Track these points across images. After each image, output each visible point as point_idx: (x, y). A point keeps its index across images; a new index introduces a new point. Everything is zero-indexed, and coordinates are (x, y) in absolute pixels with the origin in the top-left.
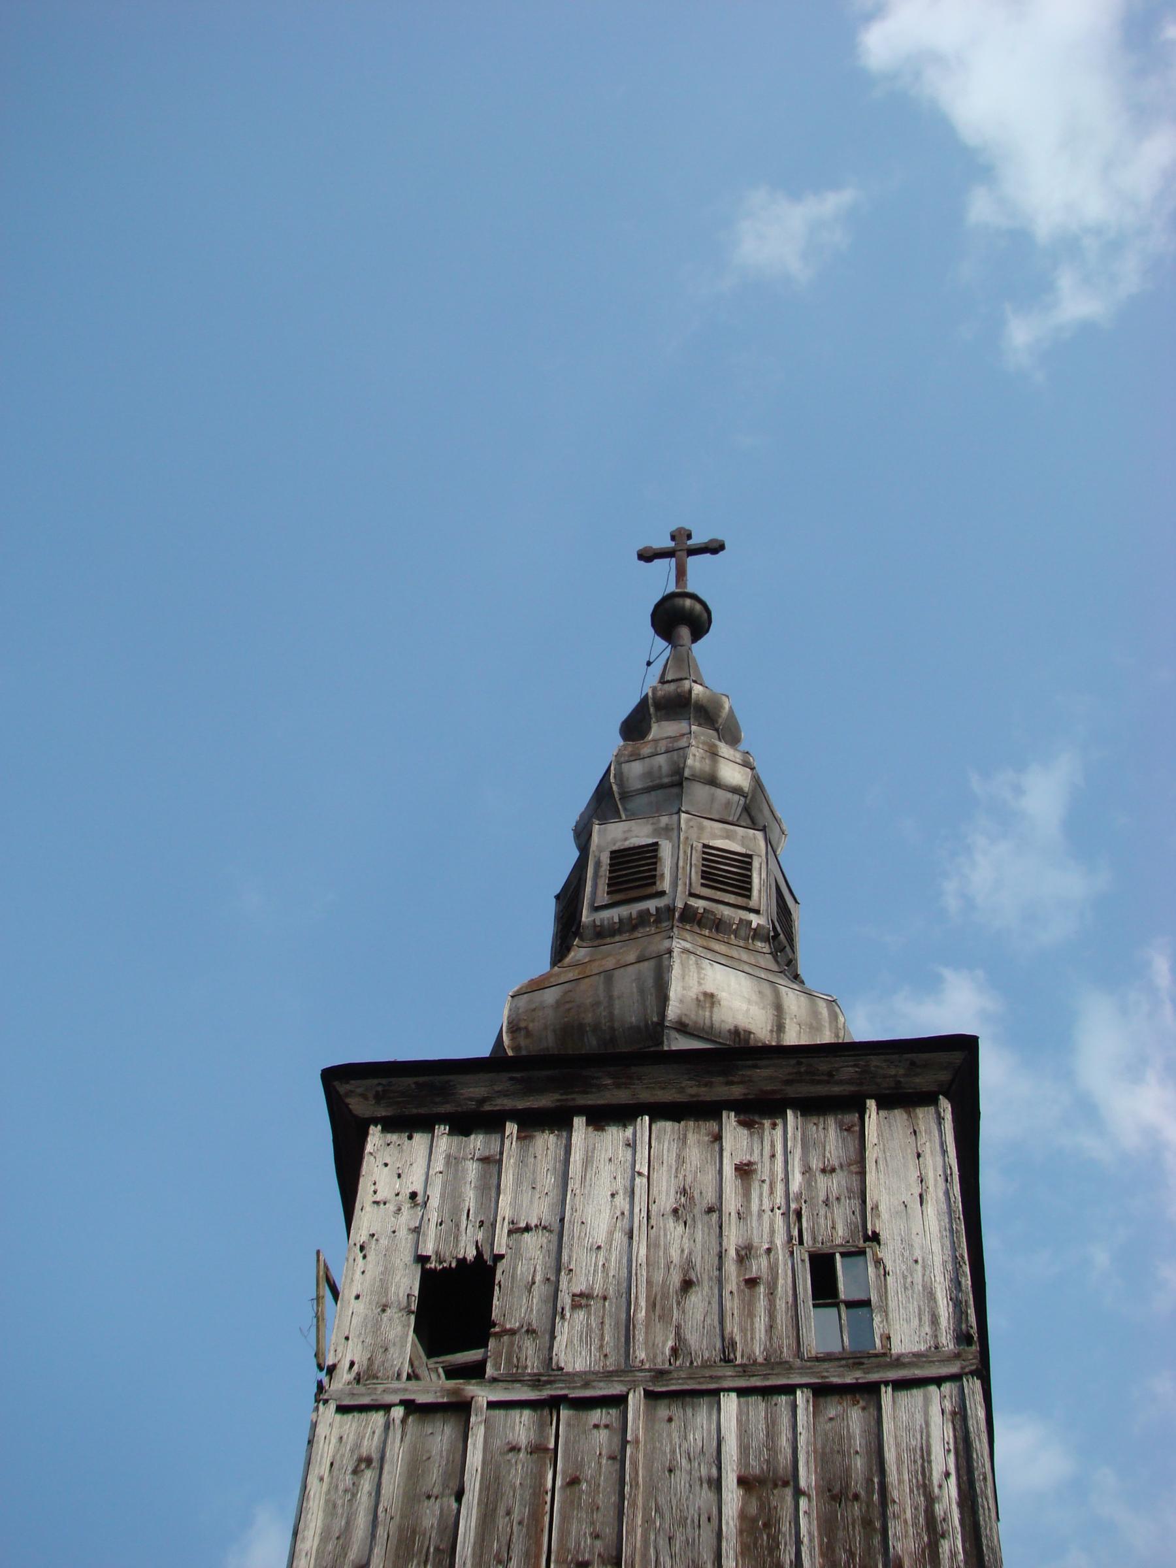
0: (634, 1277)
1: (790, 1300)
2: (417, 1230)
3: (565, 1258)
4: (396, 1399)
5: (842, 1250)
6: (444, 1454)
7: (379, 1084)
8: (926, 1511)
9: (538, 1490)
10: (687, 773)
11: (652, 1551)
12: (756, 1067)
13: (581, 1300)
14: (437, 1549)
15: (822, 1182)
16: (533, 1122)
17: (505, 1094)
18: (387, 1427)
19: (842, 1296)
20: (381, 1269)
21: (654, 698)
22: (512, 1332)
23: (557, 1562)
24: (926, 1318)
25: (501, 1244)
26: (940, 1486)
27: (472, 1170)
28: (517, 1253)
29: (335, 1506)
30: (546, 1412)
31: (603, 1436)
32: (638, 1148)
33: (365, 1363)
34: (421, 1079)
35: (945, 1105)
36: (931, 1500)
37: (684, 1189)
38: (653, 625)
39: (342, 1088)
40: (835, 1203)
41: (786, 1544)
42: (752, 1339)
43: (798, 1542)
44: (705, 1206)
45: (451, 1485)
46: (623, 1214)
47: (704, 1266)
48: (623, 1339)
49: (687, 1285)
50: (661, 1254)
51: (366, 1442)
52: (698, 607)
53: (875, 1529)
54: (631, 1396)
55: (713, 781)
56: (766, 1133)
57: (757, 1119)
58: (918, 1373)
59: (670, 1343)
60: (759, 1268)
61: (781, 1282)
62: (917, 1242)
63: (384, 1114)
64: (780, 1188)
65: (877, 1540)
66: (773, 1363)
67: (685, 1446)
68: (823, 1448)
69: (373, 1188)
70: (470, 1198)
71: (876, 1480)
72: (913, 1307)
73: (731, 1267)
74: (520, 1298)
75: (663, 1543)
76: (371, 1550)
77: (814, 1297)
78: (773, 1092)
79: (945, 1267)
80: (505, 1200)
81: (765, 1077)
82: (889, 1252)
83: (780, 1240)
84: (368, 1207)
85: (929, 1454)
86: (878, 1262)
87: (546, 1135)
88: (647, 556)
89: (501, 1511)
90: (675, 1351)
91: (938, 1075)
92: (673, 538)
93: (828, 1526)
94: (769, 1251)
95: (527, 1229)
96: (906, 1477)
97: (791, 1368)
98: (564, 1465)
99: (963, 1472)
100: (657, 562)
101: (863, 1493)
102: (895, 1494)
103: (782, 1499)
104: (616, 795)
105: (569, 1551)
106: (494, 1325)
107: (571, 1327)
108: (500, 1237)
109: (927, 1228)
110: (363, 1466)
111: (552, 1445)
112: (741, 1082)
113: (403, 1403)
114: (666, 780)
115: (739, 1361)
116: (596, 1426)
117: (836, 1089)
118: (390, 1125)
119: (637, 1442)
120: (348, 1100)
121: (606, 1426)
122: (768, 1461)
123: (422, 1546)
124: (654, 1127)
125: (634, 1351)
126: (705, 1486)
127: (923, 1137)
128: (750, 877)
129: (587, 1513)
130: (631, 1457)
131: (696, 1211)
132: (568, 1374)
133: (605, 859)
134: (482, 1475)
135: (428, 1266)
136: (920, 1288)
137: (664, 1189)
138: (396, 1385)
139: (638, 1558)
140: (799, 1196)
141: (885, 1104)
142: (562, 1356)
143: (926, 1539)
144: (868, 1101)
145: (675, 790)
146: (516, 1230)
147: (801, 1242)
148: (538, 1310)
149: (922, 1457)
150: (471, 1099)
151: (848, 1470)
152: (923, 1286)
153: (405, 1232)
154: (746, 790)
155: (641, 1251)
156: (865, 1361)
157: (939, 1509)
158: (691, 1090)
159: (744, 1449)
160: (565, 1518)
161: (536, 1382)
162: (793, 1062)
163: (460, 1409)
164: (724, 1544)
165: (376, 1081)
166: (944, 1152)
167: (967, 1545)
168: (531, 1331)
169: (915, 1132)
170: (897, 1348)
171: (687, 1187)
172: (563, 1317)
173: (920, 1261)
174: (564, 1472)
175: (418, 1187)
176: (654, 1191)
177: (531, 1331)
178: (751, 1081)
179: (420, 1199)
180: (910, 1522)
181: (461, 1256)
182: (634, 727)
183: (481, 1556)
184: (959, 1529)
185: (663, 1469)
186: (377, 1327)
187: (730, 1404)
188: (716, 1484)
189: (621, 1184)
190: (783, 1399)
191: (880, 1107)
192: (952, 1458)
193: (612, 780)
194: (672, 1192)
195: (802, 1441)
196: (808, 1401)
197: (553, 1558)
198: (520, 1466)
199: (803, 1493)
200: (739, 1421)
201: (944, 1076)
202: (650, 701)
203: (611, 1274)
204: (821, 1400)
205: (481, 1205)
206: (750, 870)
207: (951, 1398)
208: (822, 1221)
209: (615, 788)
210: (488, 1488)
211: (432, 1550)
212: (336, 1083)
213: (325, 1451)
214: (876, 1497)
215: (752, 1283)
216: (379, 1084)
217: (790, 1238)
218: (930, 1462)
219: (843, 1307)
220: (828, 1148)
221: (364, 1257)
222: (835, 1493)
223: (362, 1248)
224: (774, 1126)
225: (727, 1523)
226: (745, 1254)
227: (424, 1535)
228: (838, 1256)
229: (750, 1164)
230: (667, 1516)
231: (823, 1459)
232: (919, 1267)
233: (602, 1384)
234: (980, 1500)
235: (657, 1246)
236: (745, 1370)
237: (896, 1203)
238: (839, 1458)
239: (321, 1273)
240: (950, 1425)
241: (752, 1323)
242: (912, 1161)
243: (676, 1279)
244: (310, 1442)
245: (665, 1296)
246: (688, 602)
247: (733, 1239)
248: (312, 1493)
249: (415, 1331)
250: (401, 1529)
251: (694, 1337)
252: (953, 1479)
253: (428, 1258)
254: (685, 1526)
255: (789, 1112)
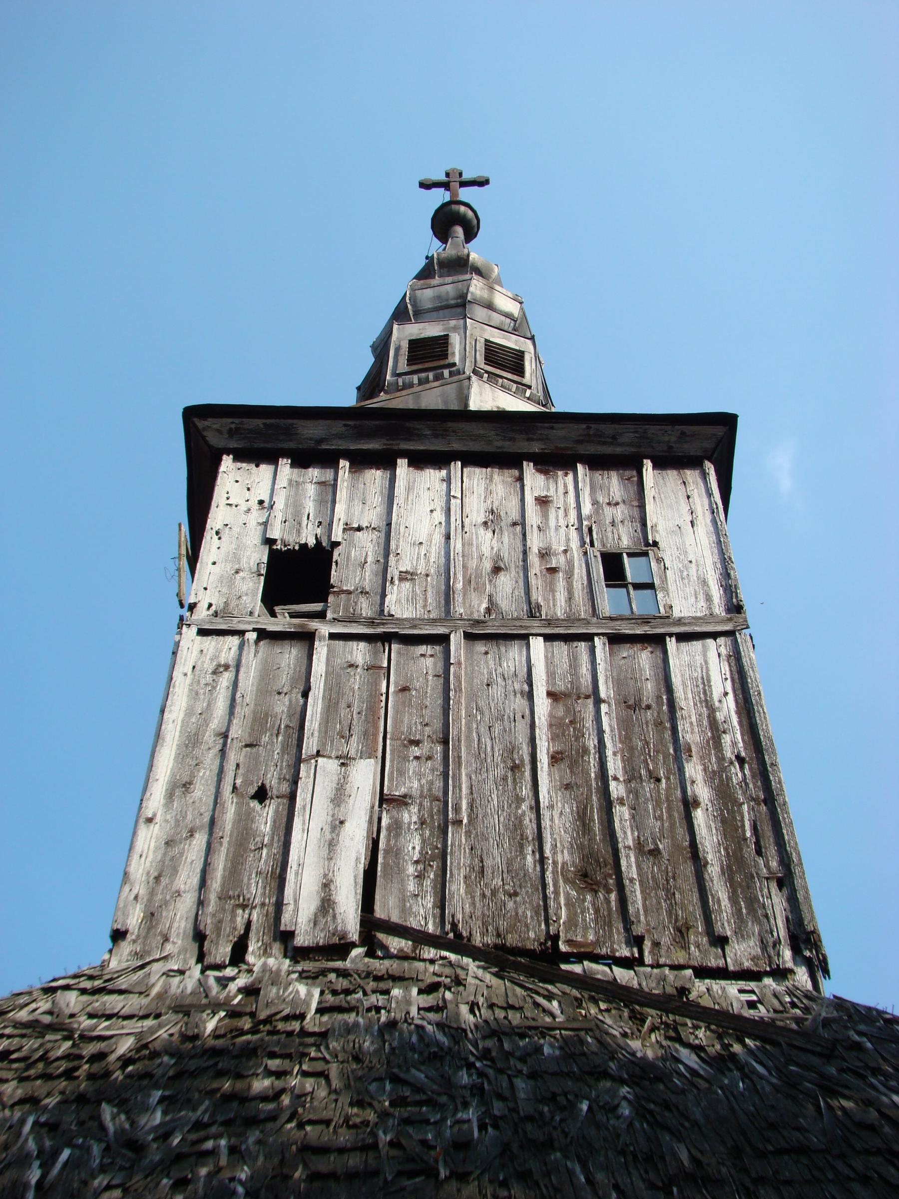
0: (452, 561)
1: (585, 583)
2: (265, 524)
3: (393, 545)
4: (250, 627)
5: (628, 551)
6: (292, 666)
7: (232, 423)
8: (709, 717)
9: (374, 694)
10: (469, 298)
11: (474, 734)
12: (552, 428)
13: (405, 576)
14: (287, 726)
15: (608, 512)
16: (362, 461)
17: (340, 436)
18: (241, 647)
19: (630, 580)
20: (234, 546)
21: (438, 259)
22: (349, 592)
23: (392, 739)
24: (701, 597)
25: (337, 534)
26: (720, 701)
27: (311, 490)
28: (351, 543)
29: (197, 694)
30: (379, 644)
31: (429, 662)
32: (453, 481)
33: (222, 605)
34: (269, 421)
35: (710, 468)
36: (712, 710)
37: (492, 510)
38: (432, 228)
39: (200, 424)
40: (620, 524)
41: (589, 735)
42: (554, 605)
43: (600, 732)
44: (510, 521)
45: (298, 686)
46: (440, 523)
47: (511, 556)
48: (443, 602)
49: (497, 570)
50: (474, 549)
51: (223, 655)
52: (470, 214)
53: (665, 728)
54: (452, 636)
55: (490, 306)
56: (560, 478)
57: (551, 468)
58: (698, 629)
59: (484, 605)
60: (558, 562)
61: (576, 571)
62: (690, 550)
63: (236, 446)
64: (573, 514)
65: (668, 735)
66: (571, 619)
67: (499, 670)
68: (619, 675)
69: (226, 495)
70: (310, 506)
71: (664, 697)
72: (689, 590)
73: (534, 559)
74: (355, 571)
75: (483, 730)
76: (230, 721)
77: (607, 579)
78: (566, 448)
79: (715, 566)
80: (340, 508)
81: (560, 435)
82: (668, 550)
83: (575, 544)
84: (222, 507)
85: (709, 681)
86: (659, 560)
87: (373, 471)
88: (426, 185)
89: (343, 705)
90: (488, 611)
91: (702, 443)
92: (447, 175)
93: (626, 727)
94: (565, 551)
95: (359, 529)
96: (690, 696)
97: (589, 623)
98: (396, 678)
99: (739, 692)
100: (434, 190)
101: (654, 705)
102: (683, 704)
103: (585, 706)
104: (411, 312)
105: (402, 733)
106: (333, 587)
107: (399, 592)
108: (337, 531)
109: (698, 541)
110: (221, 669)
111: (385, 665)
112: (539, 439)
113: (254, 630)
114: (452, 302)
115: (544, 617)
116: (422, 655)
117: (618, 450)
118: (241, 456)
119: (459, 663)
120: (205, 433)
121: (432, 656)
122: (572, 682)
123: (274, 724)
124: (465, 470)
125: (454, 608)
126: (518, 695)
127: (691, 487)
128: (523, 365)
129: (417, 710)
130: (454, 674)
131: (503, 524)
132: (397, 619)
133: (405, 345)
134: (326, 680)
135: (275, 547)
136: (696, 579)
137: (475, 509)
138: (249, 619)
139: (463, 738)
140: (589, 518)
141: (660, 464)
142: (393, 608)
143: (709, 734)
144: (645, 461)
145: (459, 310)
146: (348, 528)
147: (592, 545)
148: (370, 580)
149: (703, 683)
150: (311, 439)
151: (639, 691)
152: (698, 578)
153: (255, 523)
154: (516, 315)
155: (457, 545)
156: (652, 621)
157: (720, 716)
158: (499, 444)
159: (551, 675)
160: (397, 712)
161: (371, 622)
162: (584, 426)
163: (307, 638)
164: (537, 731)
165: (230, 420)
166: (710, 494)
167: (746, 737)
168: (364, 593)
169: (684, 483)
170: (676, 613)
171: (495, 509)
172: (392, 582)
173: (694, 561)
174: (396, 683)
175: (266, 497)
176: (467, 510)
177: (364, 593)
178: (547, 439)
179: (266, 504)
180: (695, 724)
181: (303, 542)
182: (426, 273)
183: (326, 732)
184: (738, 728)
185: (482, 683)
186: (231, 582)
187: (538, 645)
188: (530, 696)
189: (439, 504)
190: (583, 646)
191: (655, 467)
192: (729, 684)
193: (408, 301)
194: (482, 511)
195: (601, 669)
196: (604, 644)
197: (388, 736)
198: (358, 677)
199: (604, 701)
200: (546, 657)
201: (709, 445)
202: (435, 261)
203: (432, 560)
204: (615, 647)
205: (319, 512)
206: (523, 361)
207: (726, 646)
208: (610, 535)
209: (409, 306)
210: (331, 690)
211: (282, 727)
212: (196, 420)
213: (184, 665)
214: (665, 708)
215: (553, 571)
216: (232, 423)
217: (583, 543)
218: (710, 686)
219: (631, 588)
220: (612, 490)
221: (220, 538)
222: (631, 705)
223: (217, 533)
224: (566, 475)
225: (540, 718)
226: (544, 554)
227: (276, 717)
228: (625, 555)
229: (546, 497)
230: (487, 713)
231: (618, 683)
232: (693, 565)
233: (427, 627)
234: (755, 708)
235: (470, 544)
236: (549, 622)
237: (671, 525)
238: (632, 683)
239: (183, 539)
240: (726, 663)
241: (554, 596)
242: (683, 501)
243: (488, 565)
244: (174, 653)
245: (479, 575)
246: (462, 209)
247: (535, 542)
248: (177, 683)
249: (262, 601)
250: (254, 712)
251: (505, 602)
252: (731, 697)
253: (276, 540)
254: (502, 720)
255: (580, 467)
